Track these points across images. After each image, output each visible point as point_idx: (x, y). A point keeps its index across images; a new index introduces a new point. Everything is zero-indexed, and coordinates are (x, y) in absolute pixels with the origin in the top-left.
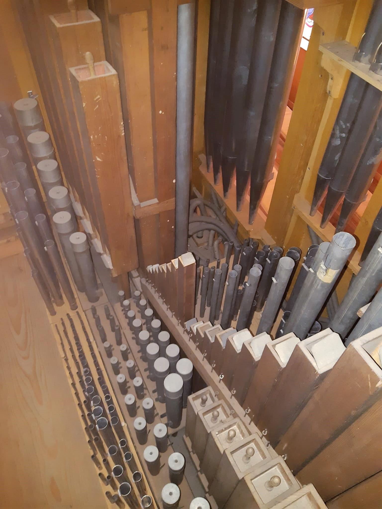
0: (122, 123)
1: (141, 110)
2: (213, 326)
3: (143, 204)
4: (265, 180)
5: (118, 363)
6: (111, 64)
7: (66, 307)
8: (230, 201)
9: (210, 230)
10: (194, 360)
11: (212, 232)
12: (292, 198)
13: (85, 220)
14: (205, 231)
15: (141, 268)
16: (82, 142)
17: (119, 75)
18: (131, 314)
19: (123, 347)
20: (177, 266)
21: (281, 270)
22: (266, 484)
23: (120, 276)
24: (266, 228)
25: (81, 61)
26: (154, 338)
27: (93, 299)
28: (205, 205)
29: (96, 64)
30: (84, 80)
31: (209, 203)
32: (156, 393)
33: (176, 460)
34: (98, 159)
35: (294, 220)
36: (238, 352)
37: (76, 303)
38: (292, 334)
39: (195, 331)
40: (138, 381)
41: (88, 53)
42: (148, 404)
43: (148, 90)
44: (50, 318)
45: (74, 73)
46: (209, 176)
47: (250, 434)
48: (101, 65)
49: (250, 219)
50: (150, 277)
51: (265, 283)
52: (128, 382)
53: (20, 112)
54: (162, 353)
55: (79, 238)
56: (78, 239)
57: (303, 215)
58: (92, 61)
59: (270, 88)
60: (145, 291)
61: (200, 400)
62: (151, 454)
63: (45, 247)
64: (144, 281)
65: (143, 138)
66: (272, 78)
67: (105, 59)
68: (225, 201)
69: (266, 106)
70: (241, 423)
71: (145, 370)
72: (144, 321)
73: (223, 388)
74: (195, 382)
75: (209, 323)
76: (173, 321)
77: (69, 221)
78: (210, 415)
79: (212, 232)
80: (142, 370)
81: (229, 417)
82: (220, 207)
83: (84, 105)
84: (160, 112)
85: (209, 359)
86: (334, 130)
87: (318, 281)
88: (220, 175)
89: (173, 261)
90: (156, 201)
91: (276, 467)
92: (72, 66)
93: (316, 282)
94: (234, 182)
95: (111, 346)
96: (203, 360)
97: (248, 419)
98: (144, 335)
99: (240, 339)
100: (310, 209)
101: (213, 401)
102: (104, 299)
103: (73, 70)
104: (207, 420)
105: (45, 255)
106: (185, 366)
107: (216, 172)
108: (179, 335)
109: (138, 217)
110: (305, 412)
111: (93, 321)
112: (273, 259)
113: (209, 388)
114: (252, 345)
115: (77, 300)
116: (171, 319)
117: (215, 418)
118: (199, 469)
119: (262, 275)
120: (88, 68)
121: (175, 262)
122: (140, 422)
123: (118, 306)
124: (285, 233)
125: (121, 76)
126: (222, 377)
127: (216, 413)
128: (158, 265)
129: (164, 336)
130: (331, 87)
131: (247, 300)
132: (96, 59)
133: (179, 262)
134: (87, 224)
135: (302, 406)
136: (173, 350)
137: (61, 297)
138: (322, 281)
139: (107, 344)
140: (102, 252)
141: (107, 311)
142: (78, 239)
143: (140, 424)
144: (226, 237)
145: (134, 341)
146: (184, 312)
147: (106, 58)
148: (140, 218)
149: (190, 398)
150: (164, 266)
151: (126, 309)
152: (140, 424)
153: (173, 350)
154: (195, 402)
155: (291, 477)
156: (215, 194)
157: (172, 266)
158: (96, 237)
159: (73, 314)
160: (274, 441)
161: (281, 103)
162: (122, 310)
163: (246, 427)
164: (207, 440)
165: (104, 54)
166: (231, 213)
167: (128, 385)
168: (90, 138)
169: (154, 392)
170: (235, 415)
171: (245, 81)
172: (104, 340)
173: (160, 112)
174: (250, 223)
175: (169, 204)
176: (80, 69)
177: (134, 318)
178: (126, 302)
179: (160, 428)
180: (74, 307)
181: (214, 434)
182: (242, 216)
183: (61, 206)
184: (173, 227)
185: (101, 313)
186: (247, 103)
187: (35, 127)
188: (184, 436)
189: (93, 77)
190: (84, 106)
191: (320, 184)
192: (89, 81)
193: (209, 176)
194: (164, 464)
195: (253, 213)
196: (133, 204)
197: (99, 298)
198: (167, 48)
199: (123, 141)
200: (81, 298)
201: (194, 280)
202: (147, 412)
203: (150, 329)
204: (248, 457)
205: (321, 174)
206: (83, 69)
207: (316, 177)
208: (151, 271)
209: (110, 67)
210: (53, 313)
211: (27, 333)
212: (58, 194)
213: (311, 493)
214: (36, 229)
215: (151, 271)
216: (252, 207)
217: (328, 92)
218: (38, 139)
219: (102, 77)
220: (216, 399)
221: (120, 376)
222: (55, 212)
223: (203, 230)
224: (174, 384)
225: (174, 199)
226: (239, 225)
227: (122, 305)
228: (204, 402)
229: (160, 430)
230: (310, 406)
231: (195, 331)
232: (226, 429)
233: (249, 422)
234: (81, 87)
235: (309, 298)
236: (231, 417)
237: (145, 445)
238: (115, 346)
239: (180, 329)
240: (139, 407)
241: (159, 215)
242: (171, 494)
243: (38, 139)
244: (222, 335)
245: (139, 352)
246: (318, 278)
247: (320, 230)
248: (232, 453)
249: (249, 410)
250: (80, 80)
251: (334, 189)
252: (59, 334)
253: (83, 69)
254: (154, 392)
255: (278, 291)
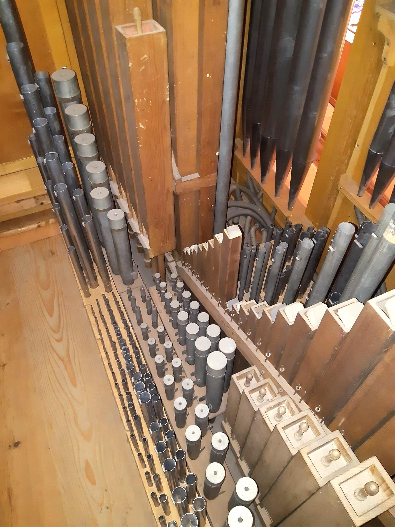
0: (168, 87)
1: (188, 74)
2: (257, 303)
3: (184, 179)
4: (308, 160)
5: (155, 345)
6: (158, 22)
7: (101, 288)
8: (268, 186)
9: (246, 216)
10: (237, 340)
11: (249, 218)
12: (337, 179)
13: (121, 199)
14: (241, 217)
15: (178, 251)
16: (124, 109)
17: (167, 33)
18: (168, 295)
19: (161, 329)
20: (221, 241)
21: (340, 236)
22: (323, 460)
23: (156, 257)
24: (306, 214)
25: (129, 18)
26: (193, 318)
27: (128, 282)
28: (241, 191)
29: (143, 22)
30: (131, 36)
31: (245, 189)
32: (194, 377)
33: (219, 441)
34: (142, 126)
35: (339, 201)
36: (290, 324)
37: (111, 286)
38: (354, 300)
39: (238, 311)
40: (177, 362)
41: (136, 8)
42: (188, 384)
43: (195, 51)
44: (84, 299)
45: (121, 30)
46: (246, 161)
47: (300, 411)
48: (148, 23)
49: (289, 204)
50: (187, 259)
51: (317, 258)
52: (166, 364)
53: (58, 83)
54: (203, 332)
55: (117, 215)
56: (115, 216)
57: (351, 196)
58: (140, 18)
59: (318, 58)
60: (181, 276)
61: (245, 379)
62: (193, 433)
63: (83, 223)
64: (180, 264)
65: (188, 105)
66: (320, 48)
67: (152, 17)
68: (263, 186)
69: (313, 78)
70: (290, 401)
71: (183, 353)
72: (182, 304)
73: (269, 366)
74: (238, 362)
75: (253, 301)
76: (213, 302)
77: (107, 197)
78: (257, 394)
79: (249, 218)
80: (179, 353)
81: (276, 396)
82: (256, 194)
83: (130, 64)
84: (208, 75)
85: (253, 339)
86: (389, 99)
87: (384, 243)
88: (258, 159)
89: (216, 236)
90: (197, 175)
91: (333, 442)
92: (118, 24)
93: (382, 244)
94: (273, 167)
95: (147, 328)
96: (247, 340)
97: (297, 398)
98: (183, 316)
99: (291, 312)
100: (357, 189)
101: (258, 380)
102: (139, 282)
103: (119, 28)
104: (254, 398)
105: (81, 231)
106: (228, 346)
107: (253, 155)
108: (220, 316)
109: (178, 192)
110: (371, 378)
111: (128, 304)
112: (319, 239)
113: (254, 368)
114: (307, 314)
115: (112, 282)
116: (210, 300)
117: (262, 396)
118: (238, 455)
119: (314, 247)
120: (135, 26)
121: (219, 237)
122: (180, 402)
123: (153, 290)
124: (328, 218)
125: (169, 34)
126: (268, 355)
127: (263, 391)
128: (196, 245)
129: (203, 317)
130: (387, 53)
131: (296, 276)
132: (144, 17)
133: (225, 237)
134: (123, 202)
135: (365, 375)
136: (213, 330)
137: (96, 279)
138: (390, 243)
139: (143, 326)
140: (138, 232)
141: (143, 292)
142: (115, 216)
143: (180, 404)
144: (264, 224)
145: (171, 324)
146: (226, 291)
147: (153, 17)
148: (180, 193)
149: (234, 376)
150: (205, 245)
151: (162, 292)
152: (180, 404)
153: (213, 330)
154: (239, 381)
155: (350, 452)
156: (251, 178)
157: (216, 242)
158: (133, 217)
159: (109, 296)
160: (328, 420)
161: (329, 75)
162: (158, 293)
163: (296, 406)
164: (253, 419)
165: (151, 11)
166: (269, 198)
167: (166, 367)
168: (134, 102)
169: (192, 375)
170: (283, 393)
171: (289, 54)
172: (140, 322)
173: (208, 75)
174: (289, 208)
175: (210, 180)
176: (126, 27)
177: (171, 299)
178: (163, 284)
179: (201, 408)
180: (108, 289)
181: (263, 411)
182: (281, 201)
183: (99, 182)
184: (213, 206)
185: (137, 295)
186: (292, 79)
187: (73, 100)
188: (223, 422)
189: (140, 34)
190: (130, 66)
191: (371, 161)
192: (137, 38)
193: (246, 161)
194: (204, 447)
195: (293, 198)
196: (173, 178)
197: (134, 280)
198: (219, 4)
199: (167, 108)
200: (116, 280)
201: (239, 255)
202: (186, 393)
203: (189, 311)
204: (301, 433)
205: (373, 150)
206: (129, 27)
207: (368, 150)
208: (189, 252)
209: (158, 25)
210: (88, 295)
211: (60, 315)
212: (96, 169)
213: (374, 467)
214: (73, 204)
215: (189, 252)
216: (293, 190)
217: (383, 59)
218: (76, 112)
219: (150, 35)
220: (261, 378)
221: (157, 357)
222: (92, 188)
223: (239, 216)
224: (217, 362)
225: (216, 174)
226: (276, 211)
227: (158, 288)
228: (248, 381)
229: (202, 411)
230: (379, 370)
231: (238, 311)
232: (275, 406)
233: (299, 400)
234: (128, 44)
235: (372, 264)
236: (279, 396)
237: (185, 428)
238: (151, 328)
239: (221, 310)
240: (177, 389)
241: (199, 191)
242: (215, 473)
243: (76, 112)
244: (271, 310)
245: (176, 335)
246: (385, 239)
247: (369, 210)
248: (284, 428)
249: (300, 387)
250: (127, 37)
251: (388, 164)
252: (94, 315)
253: (129, 27)
254: (192, 375)
255: (335, 261)
